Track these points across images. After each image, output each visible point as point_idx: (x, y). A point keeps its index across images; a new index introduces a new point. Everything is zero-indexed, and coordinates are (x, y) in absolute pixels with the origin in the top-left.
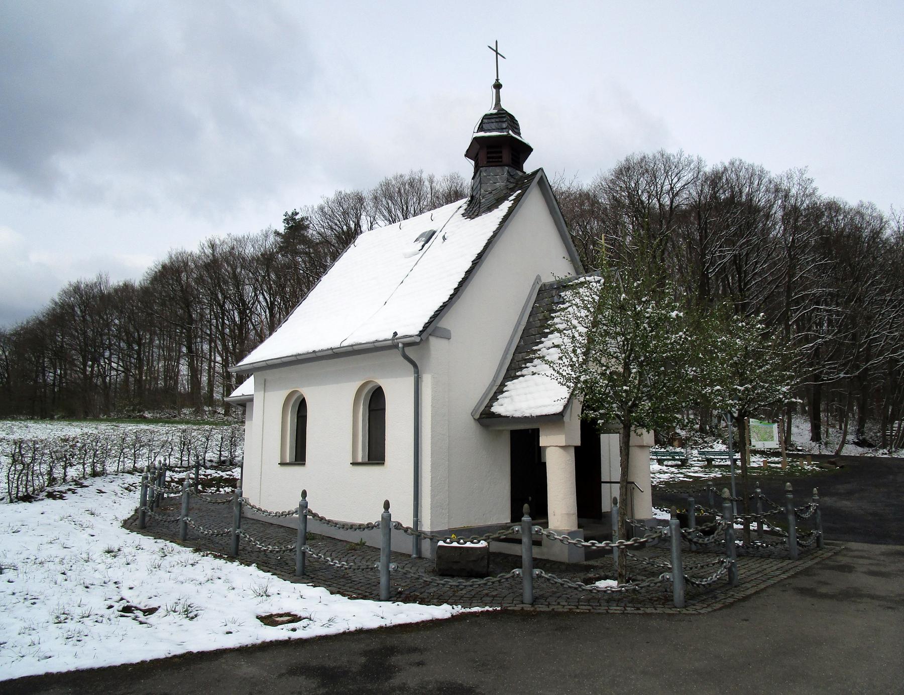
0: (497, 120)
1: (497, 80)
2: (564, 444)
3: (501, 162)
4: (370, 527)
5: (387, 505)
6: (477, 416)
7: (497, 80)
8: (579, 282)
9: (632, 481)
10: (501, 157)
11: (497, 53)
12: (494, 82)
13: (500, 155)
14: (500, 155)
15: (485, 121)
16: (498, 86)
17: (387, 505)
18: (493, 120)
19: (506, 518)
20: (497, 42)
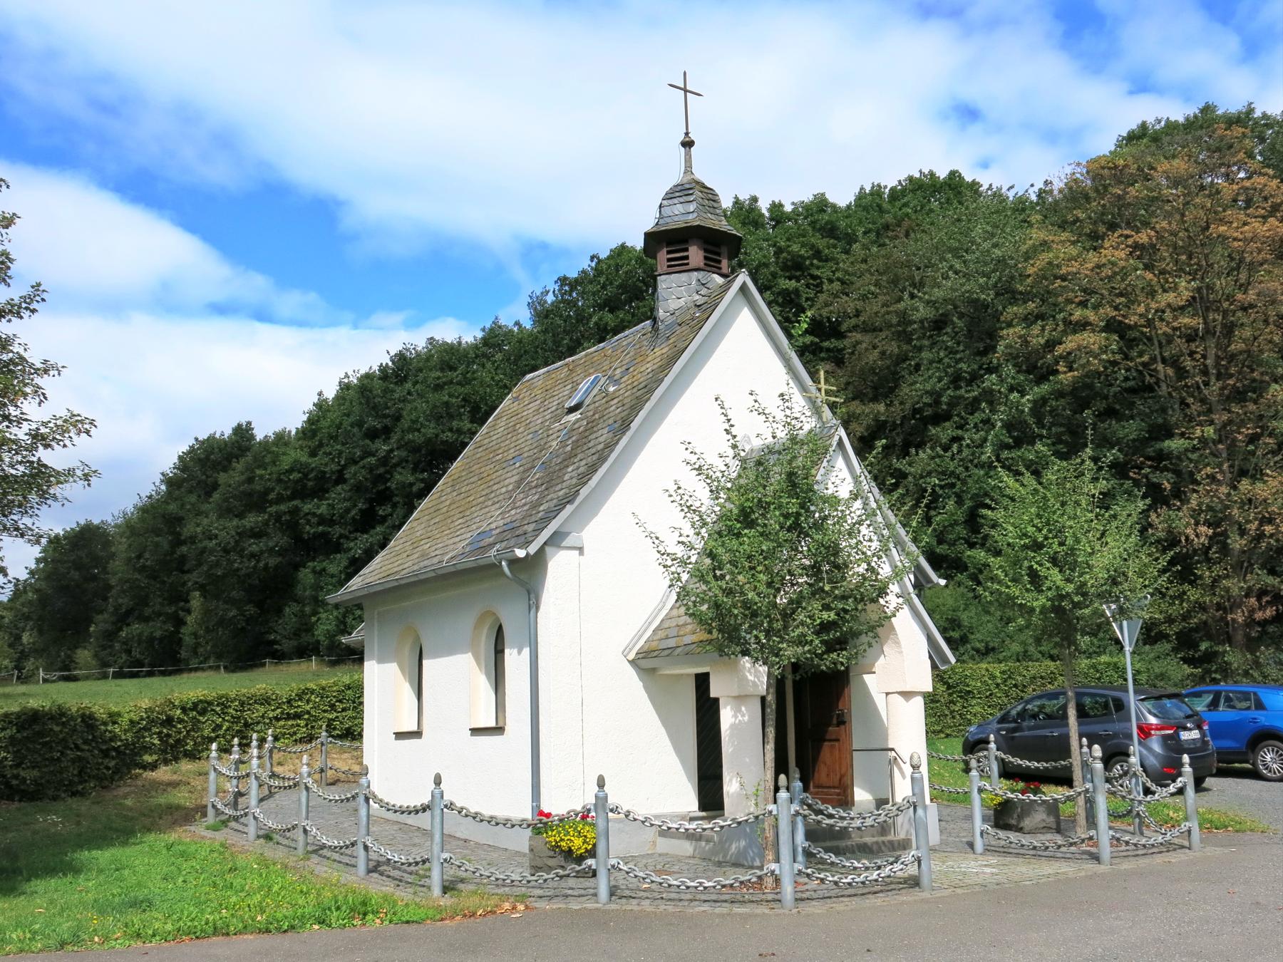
0: (682, 200)
1: (687, 134)
2: (736, 694)
3: (688, 264)
4: (508, 823)
5: (438, 781)
6: (632, 656)
7: (687, 134)
8: (897, 412)
9: (890, 746)
10: (687, 258)
11: (686, 91)
12: (682, 137)
13: (685, 254)
14: (685, 254)
15: (665, 203)
16: (688, 144)
17: (438, 781)
18: (676, 201)
19: (689, 802)
20: (685, 73)
